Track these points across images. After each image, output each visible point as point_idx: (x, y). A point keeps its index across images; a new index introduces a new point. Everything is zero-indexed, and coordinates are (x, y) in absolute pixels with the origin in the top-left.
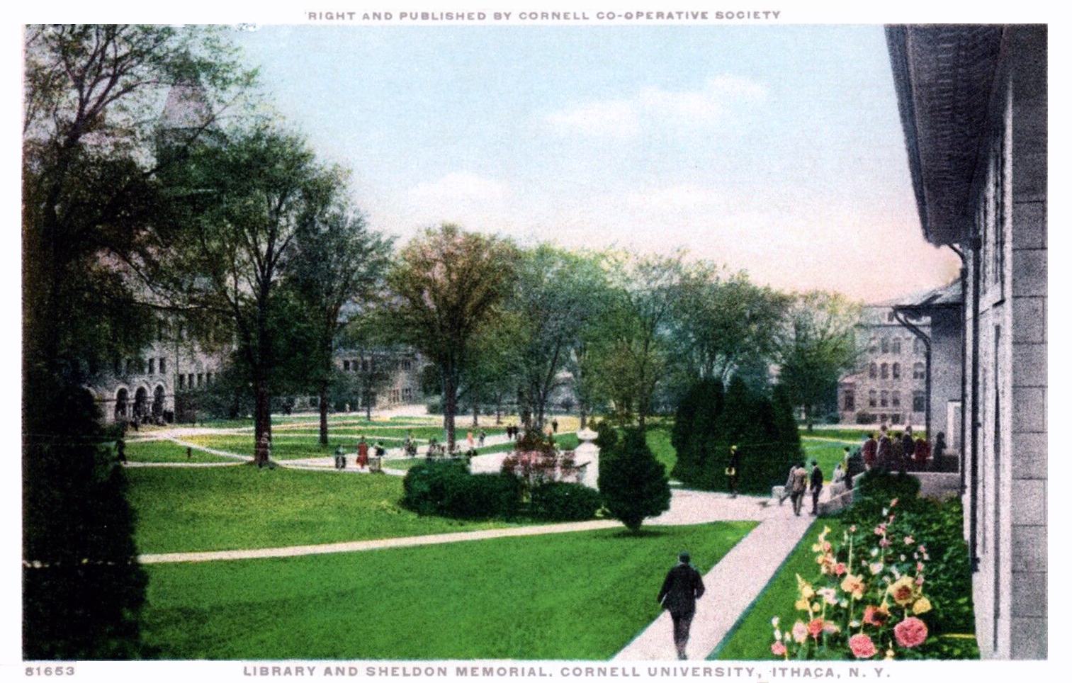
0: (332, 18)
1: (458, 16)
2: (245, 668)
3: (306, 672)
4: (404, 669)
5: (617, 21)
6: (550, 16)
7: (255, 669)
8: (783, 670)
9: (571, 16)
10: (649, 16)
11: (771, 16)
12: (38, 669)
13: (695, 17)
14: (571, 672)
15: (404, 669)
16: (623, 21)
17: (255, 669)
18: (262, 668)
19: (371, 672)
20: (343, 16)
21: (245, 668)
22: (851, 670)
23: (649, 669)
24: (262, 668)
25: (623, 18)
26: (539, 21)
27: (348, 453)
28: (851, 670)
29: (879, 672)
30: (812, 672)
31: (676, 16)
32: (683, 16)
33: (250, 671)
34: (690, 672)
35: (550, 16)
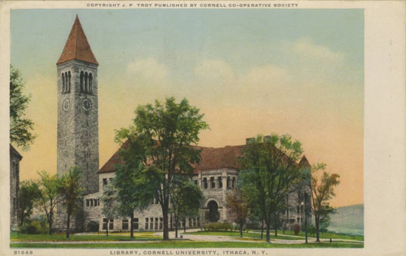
0: (111, 6)
1: (177, 5)
2: (111, 252)
3: (134, 253)
4: (167, 252)
5: (236, 7)
6: (211, 5)
7: (207, 254)
8: (210, 252)
9: (219, 5)
10: (248, 6)
11: (294, 5)
12: (19, 252)
13: (266, 6)
14: (147, 253)
15: (167, 252)
16: (239, 7)
17: (207, 254)
18: (117, 252)
19: (23, 252)
20: (115, 5)
21: (111, 252)
22: (253, 252)
23: (177, 252)
24: (117, 252)
25: (239, 6)
26: (207, 7)
27: (157, 141)
28: (253, 252)
29: (263, 252)
30: (238, 252)
31: (259, 6)
32: (262, 5)
33: (113, 252)
34: (192, 252)
35: (211, 5)
